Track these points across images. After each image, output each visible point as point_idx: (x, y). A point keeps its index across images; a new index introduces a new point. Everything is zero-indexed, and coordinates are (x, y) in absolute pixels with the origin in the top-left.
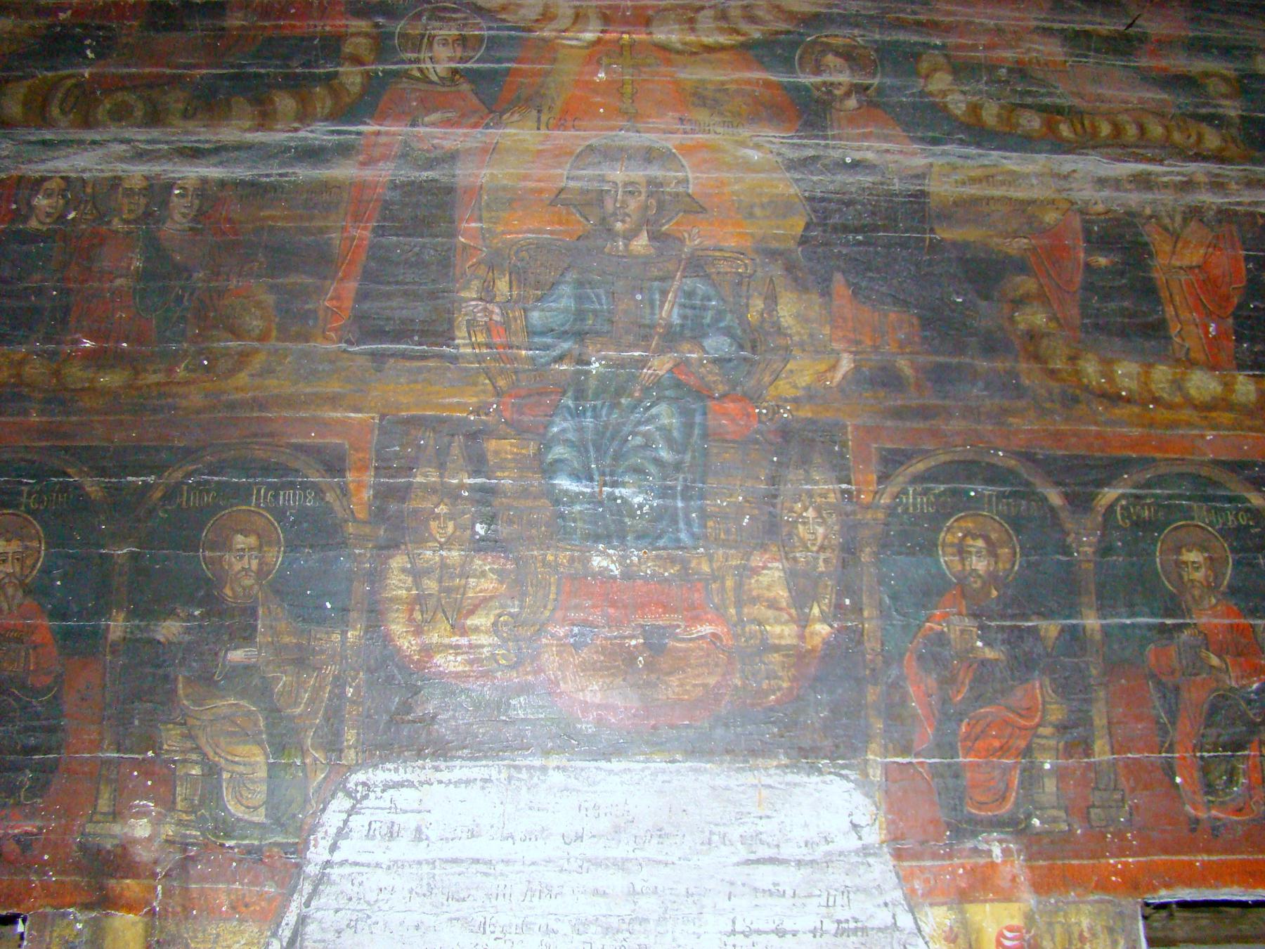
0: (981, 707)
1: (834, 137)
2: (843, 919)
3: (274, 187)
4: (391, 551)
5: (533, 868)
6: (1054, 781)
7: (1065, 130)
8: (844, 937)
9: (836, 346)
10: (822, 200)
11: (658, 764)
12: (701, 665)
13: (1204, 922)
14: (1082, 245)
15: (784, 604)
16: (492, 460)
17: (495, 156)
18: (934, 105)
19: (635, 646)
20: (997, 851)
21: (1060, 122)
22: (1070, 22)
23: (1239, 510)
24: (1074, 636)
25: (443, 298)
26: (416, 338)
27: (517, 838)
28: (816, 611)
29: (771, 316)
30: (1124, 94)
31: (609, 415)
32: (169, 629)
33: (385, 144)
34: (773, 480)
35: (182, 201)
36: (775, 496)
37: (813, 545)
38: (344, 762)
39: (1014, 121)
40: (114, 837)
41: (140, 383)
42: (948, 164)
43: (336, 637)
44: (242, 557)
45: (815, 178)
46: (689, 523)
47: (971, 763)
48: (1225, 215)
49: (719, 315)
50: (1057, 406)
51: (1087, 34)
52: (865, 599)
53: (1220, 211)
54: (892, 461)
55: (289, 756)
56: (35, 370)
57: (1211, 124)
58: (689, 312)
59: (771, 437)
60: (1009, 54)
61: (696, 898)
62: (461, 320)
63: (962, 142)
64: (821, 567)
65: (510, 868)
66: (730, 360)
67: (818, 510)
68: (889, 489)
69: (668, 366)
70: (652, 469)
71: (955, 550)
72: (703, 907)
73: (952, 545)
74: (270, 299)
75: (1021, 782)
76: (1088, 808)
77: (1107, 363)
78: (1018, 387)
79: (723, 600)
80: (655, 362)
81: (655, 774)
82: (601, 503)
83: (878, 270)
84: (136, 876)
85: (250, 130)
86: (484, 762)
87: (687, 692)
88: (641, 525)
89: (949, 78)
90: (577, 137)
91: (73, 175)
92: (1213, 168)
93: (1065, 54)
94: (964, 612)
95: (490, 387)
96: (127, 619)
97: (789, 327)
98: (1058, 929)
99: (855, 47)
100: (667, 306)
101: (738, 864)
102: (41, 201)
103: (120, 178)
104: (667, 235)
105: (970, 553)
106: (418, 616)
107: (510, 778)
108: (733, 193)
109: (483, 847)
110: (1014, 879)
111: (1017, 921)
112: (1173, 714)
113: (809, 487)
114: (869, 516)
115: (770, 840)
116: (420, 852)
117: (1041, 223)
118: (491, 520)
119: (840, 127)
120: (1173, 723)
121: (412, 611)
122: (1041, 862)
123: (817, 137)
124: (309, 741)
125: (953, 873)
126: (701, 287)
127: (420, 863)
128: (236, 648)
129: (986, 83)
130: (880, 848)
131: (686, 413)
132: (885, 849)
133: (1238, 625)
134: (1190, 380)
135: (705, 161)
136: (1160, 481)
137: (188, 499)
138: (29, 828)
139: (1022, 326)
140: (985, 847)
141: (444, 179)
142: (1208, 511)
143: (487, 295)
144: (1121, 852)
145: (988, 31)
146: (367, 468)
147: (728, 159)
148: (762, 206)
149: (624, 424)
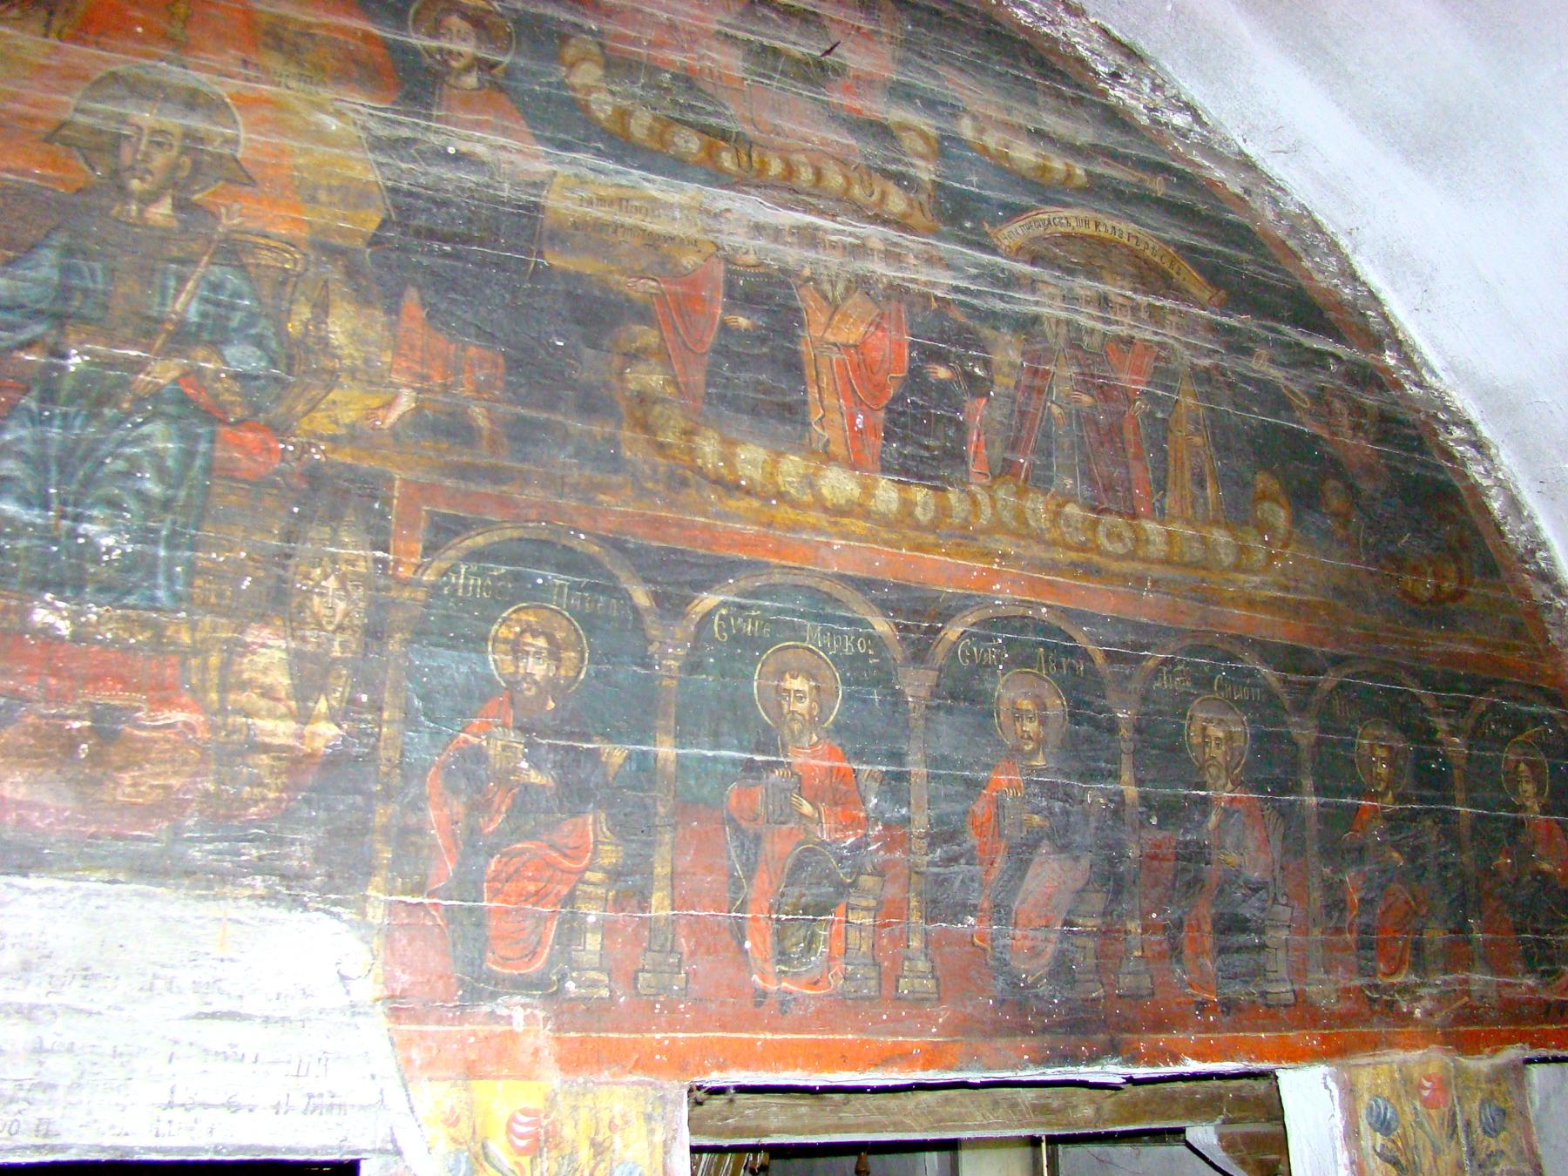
0: (518, 841)
1: (439, 119)
6: (599, 937)
7: (727, 160)
9: (396, 378)
10: (410, 194)
12: (163, 762)
13: (803, 1110)
14: (722, 299)
15: (283, 695)
18: (573, 104)
19: (79, 730)
20: (519, 1015)
21: (724, 149)
23: (858, 635)
24: (644, 766)
29: (318, 329)
30: (805, 130)
31: (83, 427)
34: (288, 536)
36: (288, 556)
37: (330, 623)
42: (576, 175)
45: (404, 166)
46: (171, 578)
48: (897, 291)
49: (252, 318)
50: (661, 487)
51: (776, 52)
52: (387, 696)
53: (890, 286)
54: (444, 531)
58: (211, 309)
59: (295, 481)
60: (677, 57)
61: (124, 1059)
63: (599, 153)
66: (257, 378)
67: (342, 580)
68: (435, 564)
69: (175, 374)
70: (131, 503)
73: (506, 641)
75: (558, 936)
76: (637, 972)
77: (729, 443)
78: (616, 458)
79: (203, 681)
80: (157, 367)
81: (87, 896)
82: (55, 541)
83: (465, 293)
87: (142, 794)
88: (105, 573)
89: (599, 72)
90: (99, 58)
92: (892, 234)
93: (746, 70)
97: (340, 347)
98: (584, 1114)
100: (183, 298)
101: (187, 1018)
104: (197, 206)
105: (528, 653)
108: (296, 167)
110: (536, 1052)
111: (537, 1103)
112: (750, 873)
113: (333, 550)
114: (406, 594)
117: (676, 265)
120: (749, 878)
122: (573, 1034)
123: (418, 115)
126: (233, 280)
129: (643, 87)
131: (188, 437)
132: (380, 1008)
133: (839, 769)
135: (264, 120)
136: (771, 591)
139: (632, 386)
140: (503, 1011)
142: (823, 633)
144: (671, 1027)
145: (659, 24)
147: (296, 122)
148: (330, 190)
149: (102, 441)
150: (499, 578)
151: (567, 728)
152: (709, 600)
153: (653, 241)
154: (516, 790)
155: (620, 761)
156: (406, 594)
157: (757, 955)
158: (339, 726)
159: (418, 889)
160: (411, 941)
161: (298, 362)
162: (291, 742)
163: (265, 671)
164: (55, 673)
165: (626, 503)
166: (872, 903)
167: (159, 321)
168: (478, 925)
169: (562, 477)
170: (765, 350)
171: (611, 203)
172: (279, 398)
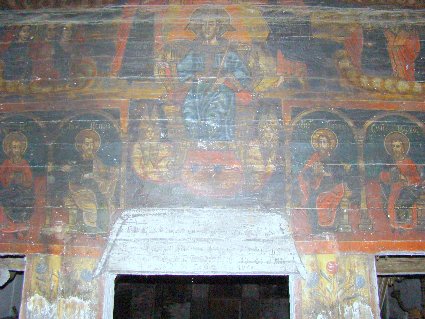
0: (324, 191)
1: (279, 4)
2: (277, 258)
3: (95, 26)
4: (135, 142)
5: (179, 241)
6: (347, 216)
9: (278, 74)
10: (275, 25)
14: (363, 39)
16: (166, 113)
17: (167, 14)
19: (211, 172)
20: (328, 238)
24: (356, 169)
25: (150, 61)
26: (142, 74)
27: (174, 232)
28: (270, 160)
31: (203, 97)
32: (66, 168)
33: (131, 11)
34: (257, 118)
35: (66, 32)
36: (257, 123)
38: (120, 208)
40: (51, 232)
41: (55, 91)
43: (117, 170)
44: (88, 145)
47: (320, 210)
48: (414, 28)
49: (240, 64)
50: (352, 93)
52: (286, 156)
53: (412, 26)
55: (103, 207)
56: (23, 88)
58: (230, 63)
62: (156, 68)
63: (323, 5)
64: (272, 146)
65: (172, 241)
66: (243, 79)
67: (271, 128)
69: (223, 81)
70: (217, 115)
72: (232, 254)
73: (315, 139)
74: (95, 63)
75: (337, 216)
77: (370, 78)
78: (339, 86)
80: (219, 80)
81: (217, 212)
82: (201, 126)
84: (58, 244)
85: (88, 8)
86: (164, 208)
91: (32, 24)
92: (411, 11)
95: (165, 89)
96: (53, 165)
97: (263, 68)
98: (347, 263)
100: (222, 62)
101: (244, 241)
102: (22, 33)
103: (47, 25)
104: (223, 38)
105: (321, 142)
106: (143, 162)
107: (172, 213)
109: (164, 235)
110: (333, 247)
111: (333, 260)
112: (388, 195)
115: (254, 233)
116: (144, 236)
118: (166, 132)
120: (388, 198)
121: (141, 161)
122: (342, 242)
123: (274, 4)
124: (110, 202)
126: (234, 55)
127: (144, 240)
128: (87, 173)
131: (229, 97)
132: (291, 236)
136: (387, 118)
137: (71, 127)
138: (26, 229)
140: (324, 236)
141: (150, 22)
142: (403, 128)
143: (164, 59)
146: (126, 116)
150: (312, 123)
151: (334, 161)
153: (342, 26)
154: (322, 178)
155: (349, 168)
156: (288, 130)
158: (275, 165)
159: (299, 206)
161: (252, 73)
162: (263, 170)
163: (255, 153)
164: (204, 158)
165: (343, 99)
167: (217, 69)
168: (315, 214)
169: (325, 94)
170: (377, 51)
171: (328, 18)
172: (250, 83)
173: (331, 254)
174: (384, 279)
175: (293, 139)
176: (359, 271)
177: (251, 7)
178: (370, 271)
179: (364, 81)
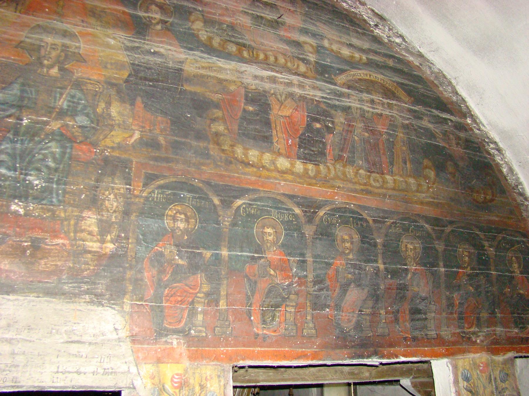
0: (175, 283)
1: (148, 40)
2: (107, 368)
7: (245, 54)
8: (107, 375)
9: (133, 127)
10: (138, 65)
11: (32, 297)
14: (243, 101)
15: (95, 234)
19: (27, 246)
20: (175, 342)
21: (244, 50)
22: (256, 12)
23: (289, 214)
24: (217, 258)
29: (107, 110)
31: (28, 144)
34: (97, 181)
36: (97, 187)
37: (111, 210)
39: (225, 46)
42: (194, 59)
45: (136, 56)
46: (58, 195)
47: (168, 306)
48: (303, 98)
49: (85, 107)
50: (223, 164)
51: (262, 18)
52: (131, 234)
53: (300, 96)
57: (303, 62)
58: (71, 104)
60: (228, 19)
63: (202, 52)
66: (87, 127)
67: (115, 195)
68: (147, 190)
69: (59, 126)
70: (44, 170)
71: (172, 218)
73: (171, 216)
75: (188, 315)
77: (246, 149)
78: (208, 154)
79: (69, 229)
81: (30, 302)
82: (19, 182)
83: (157, 98)
87: (48, 268)
88: (35, 193)
89: (202, 24)
90: (33, 19)
92: (301, 79)
93: (252, 24)
94: (172, 243)
97: (115, 117)
98: (197, 375)
99: (165, 4)
100: (62, 100)
101: (63, 343)
104: (67, 69)
105: (178, 220)
108: (100, 56)
111: (181, 372)
112: (253, 293)
115: (78, 333)
119: (151, 36)
120: (253, 296)
122: (193, 348)
123: (141, 39)
125: (156, 351)
126: (79, 94)
130: (126, 339)
131: (64, 147)
132: (128, 339)
133: (283, 259)
134: (278, 161)
136: (260, 199)
140: (170, 341)
142: (278, 213)
144: (226, 346)
148: (111, 64)
150: (168, 195)
152: (239, 202)
153: (220, 81)
154: (174, 266)
157: (255, 322)
158: (114, 244)
159: (141, 299)
160: (139, 317)
162: (98, 250)
163: (89, 226)
164: (19, 227)
166: (294, 304)
167: (54, 108)
169: (190, 161)
170: (258, 118)
171: (206, 68)
173: (178, 363)
174: (246, 390)
175: (142, 213)
176: (211, 386)
177: (112, 37)
178: (225, 386)
179: (239, 151)
